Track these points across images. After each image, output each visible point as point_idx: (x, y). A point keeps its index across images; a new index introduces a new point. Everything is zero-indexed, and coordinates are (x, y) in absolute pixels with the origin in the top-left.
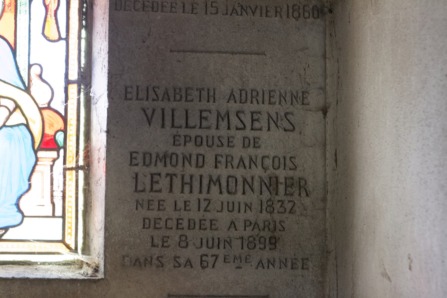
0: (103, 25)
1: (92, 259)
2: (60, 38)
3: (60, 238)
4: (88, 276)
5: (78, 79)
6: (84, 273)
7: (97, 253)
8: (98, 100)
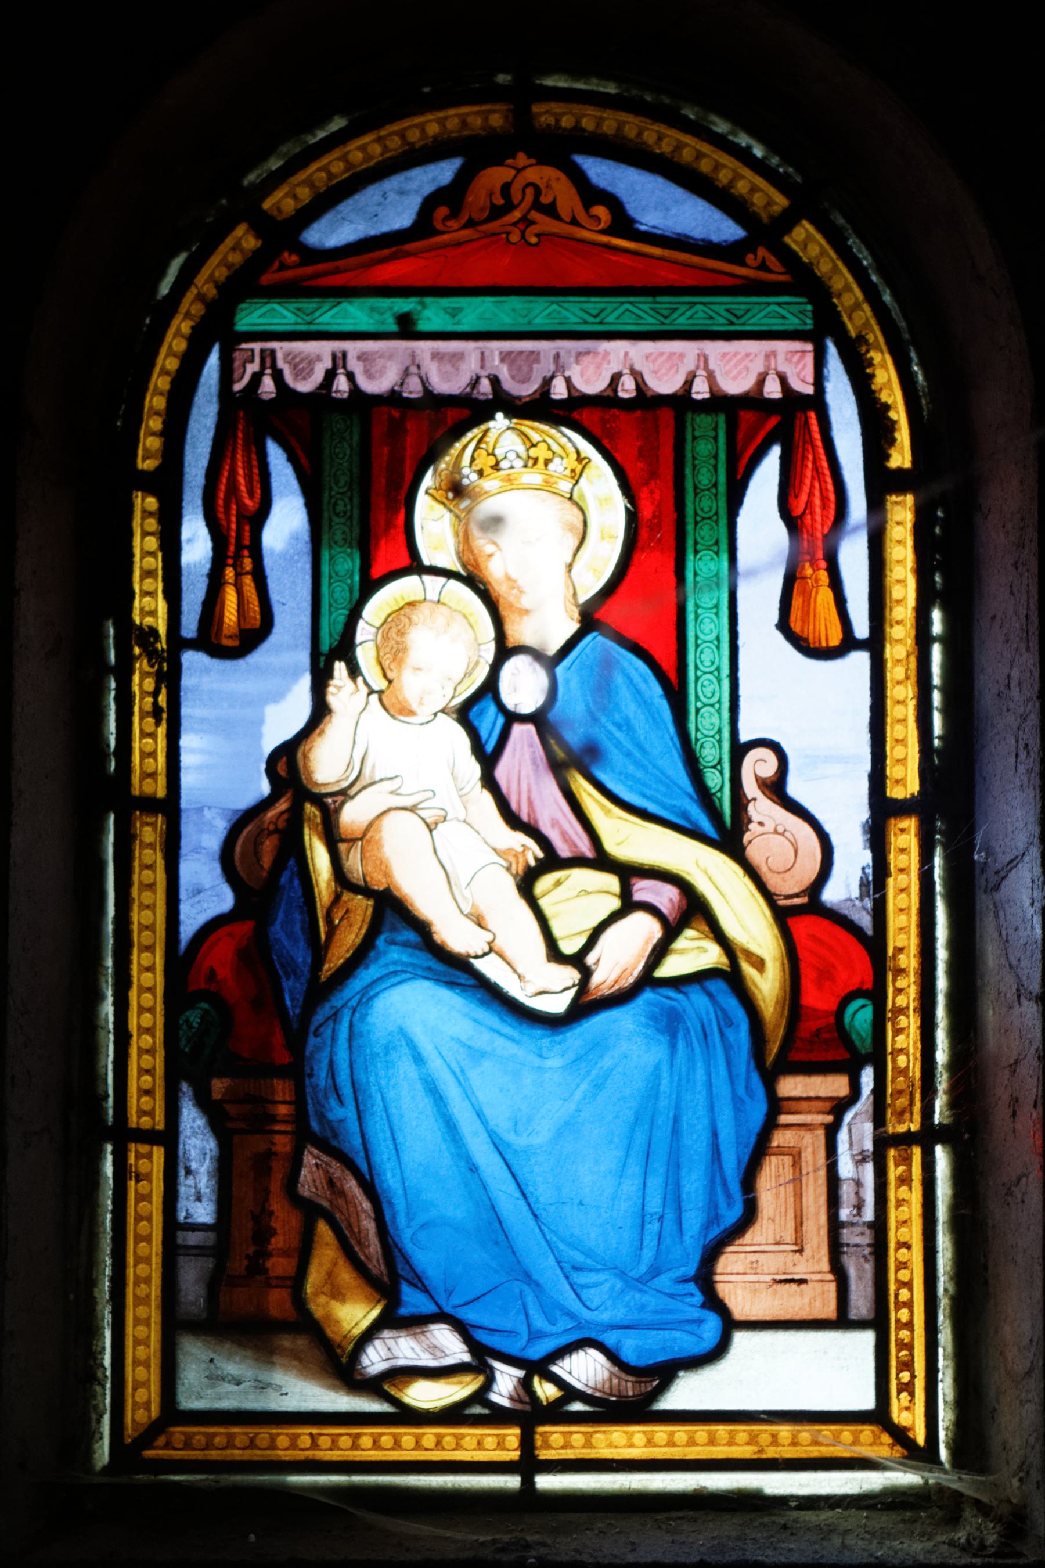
0: (1015, 589)
1: (996, 1485)
2: (849, 644)
3: (868, 1402)
4: (984, 1553)
5: (919, 792)
6: (968, 1540)
7: (1014, 1465)
8: (1002, 874)
